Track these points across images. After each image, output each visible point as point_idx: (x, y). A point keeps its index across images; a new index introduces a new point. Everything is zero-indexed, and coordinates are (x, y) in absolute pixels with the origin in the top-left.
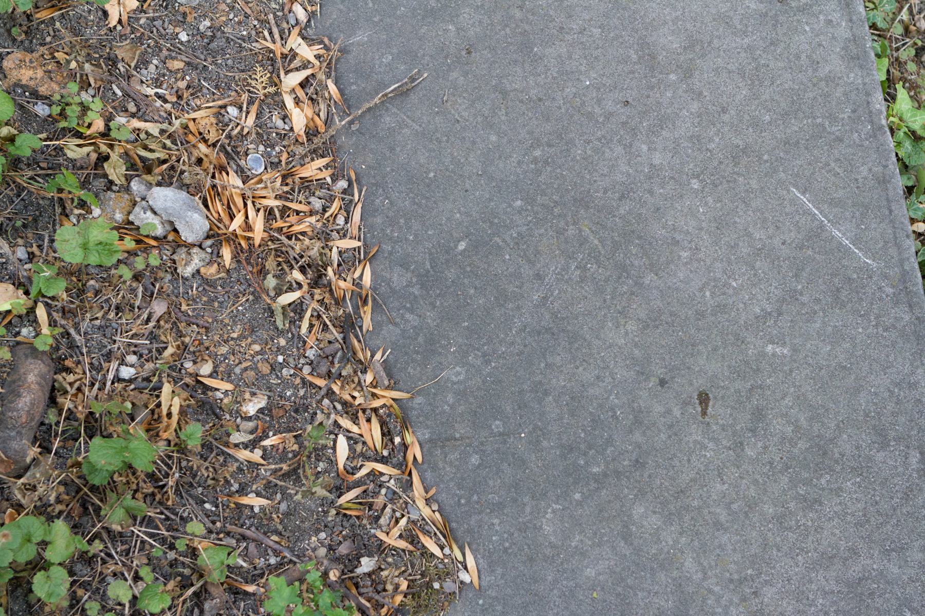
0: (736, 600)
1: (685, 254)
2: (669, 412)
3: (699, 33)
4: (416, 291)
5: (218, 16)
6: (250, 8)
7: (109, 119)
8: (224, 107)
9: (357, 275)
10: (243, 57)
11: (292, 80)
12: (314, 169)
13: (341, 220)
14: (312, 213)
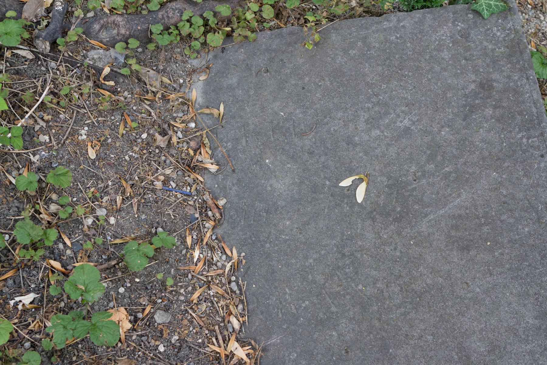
3: (497, 340)
5: (183, 330)
6: (203, 321)
10: (200, 360)
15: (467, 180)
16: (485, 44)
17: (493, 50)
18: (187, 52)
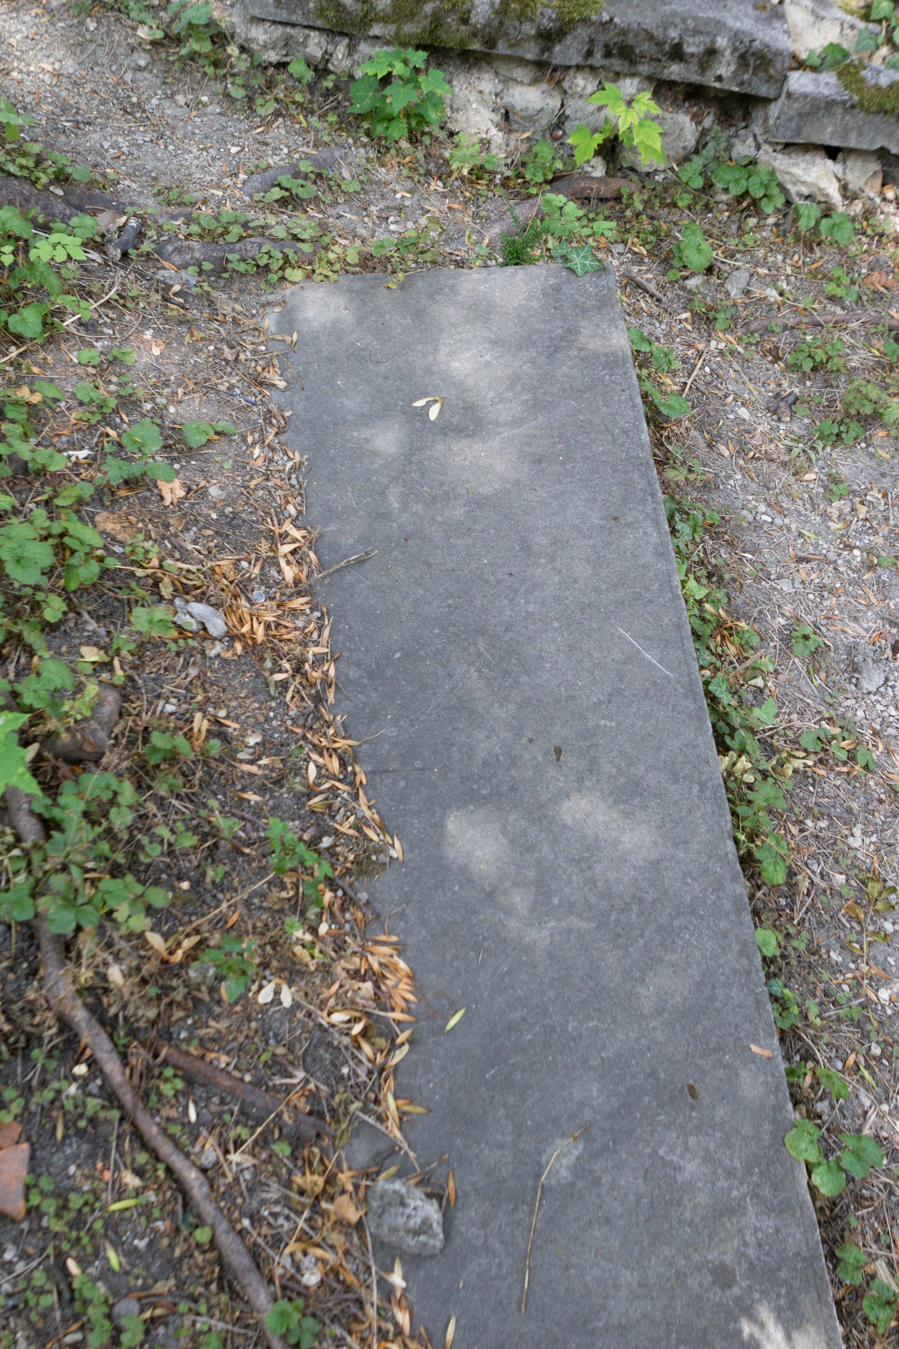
0: (576, 871)
1: (548, 665)
2: (535, 758)
4: (365, 681)
7: (162, 560)
8: (239, 560)
9: (325, 668)
11: (286, 549)
12: (298, 603)
13: (315, 636)
14: (296, 629)
15: (545, 407)
16: (577, 297)
17: (583, 303)
18: (263, 286)
